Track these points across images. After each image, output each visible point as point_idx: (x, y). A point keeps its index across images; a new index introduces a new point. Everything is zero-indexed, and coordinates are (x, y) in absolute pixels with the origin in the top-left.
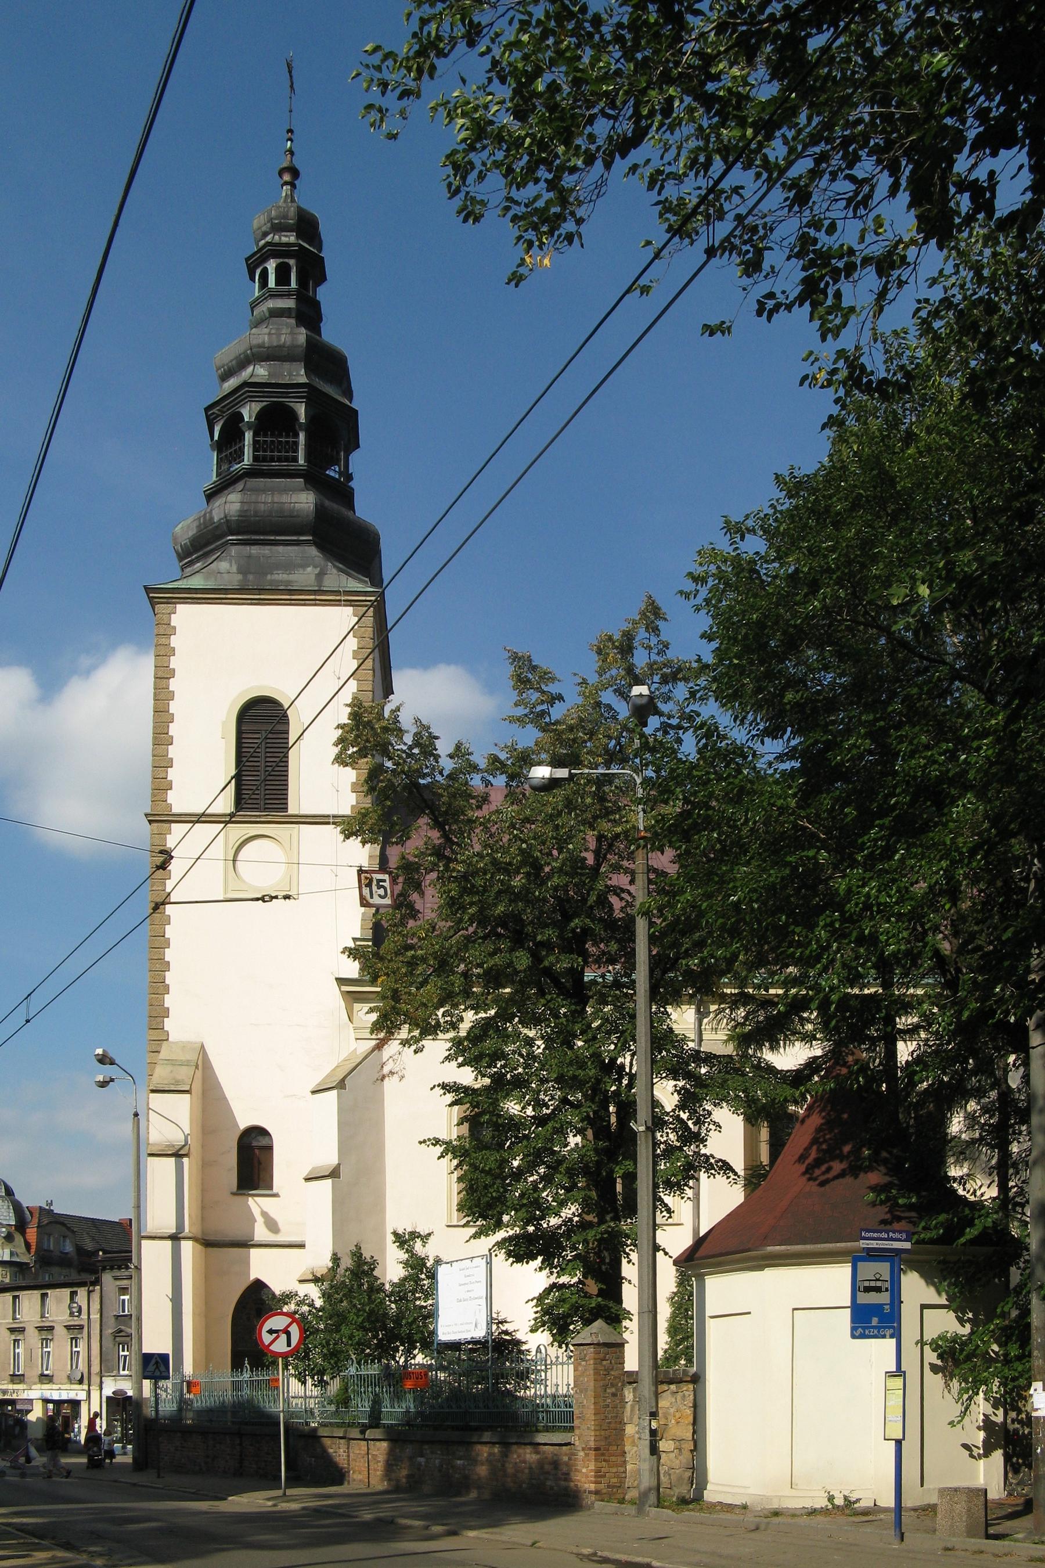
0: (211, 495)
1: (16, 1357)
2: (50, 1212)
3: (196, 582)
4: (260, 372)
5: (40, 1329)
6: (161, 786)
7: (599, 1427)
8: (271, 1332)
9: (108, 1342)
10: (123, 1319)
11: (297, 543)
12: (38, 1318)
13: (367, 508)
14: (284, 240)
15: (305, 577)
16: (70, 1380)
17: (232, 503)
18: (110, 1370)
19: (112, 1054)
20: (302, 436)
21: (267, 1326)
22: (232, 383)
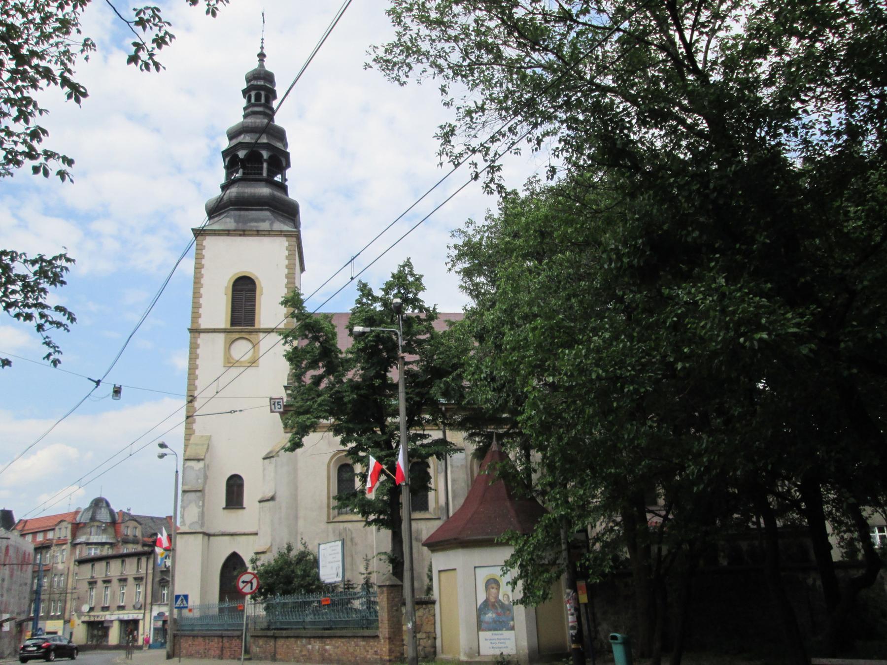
1: (106, 595)
2: (129, 514)
3: (216, 227)
4: (246, 138)
5: (135, 579)
6: (196, 316)
7: (390, 627)
8: (243, 582)
9: (156, 586)
10: (166, 572)
11: (262, 210)
14: (259, 83)
15: (265, 226)
16: (134, 607)
17: (233, 191)
18: (156, 601)
20: (265, 165)
21: (241, 580)
22: (235, 142)
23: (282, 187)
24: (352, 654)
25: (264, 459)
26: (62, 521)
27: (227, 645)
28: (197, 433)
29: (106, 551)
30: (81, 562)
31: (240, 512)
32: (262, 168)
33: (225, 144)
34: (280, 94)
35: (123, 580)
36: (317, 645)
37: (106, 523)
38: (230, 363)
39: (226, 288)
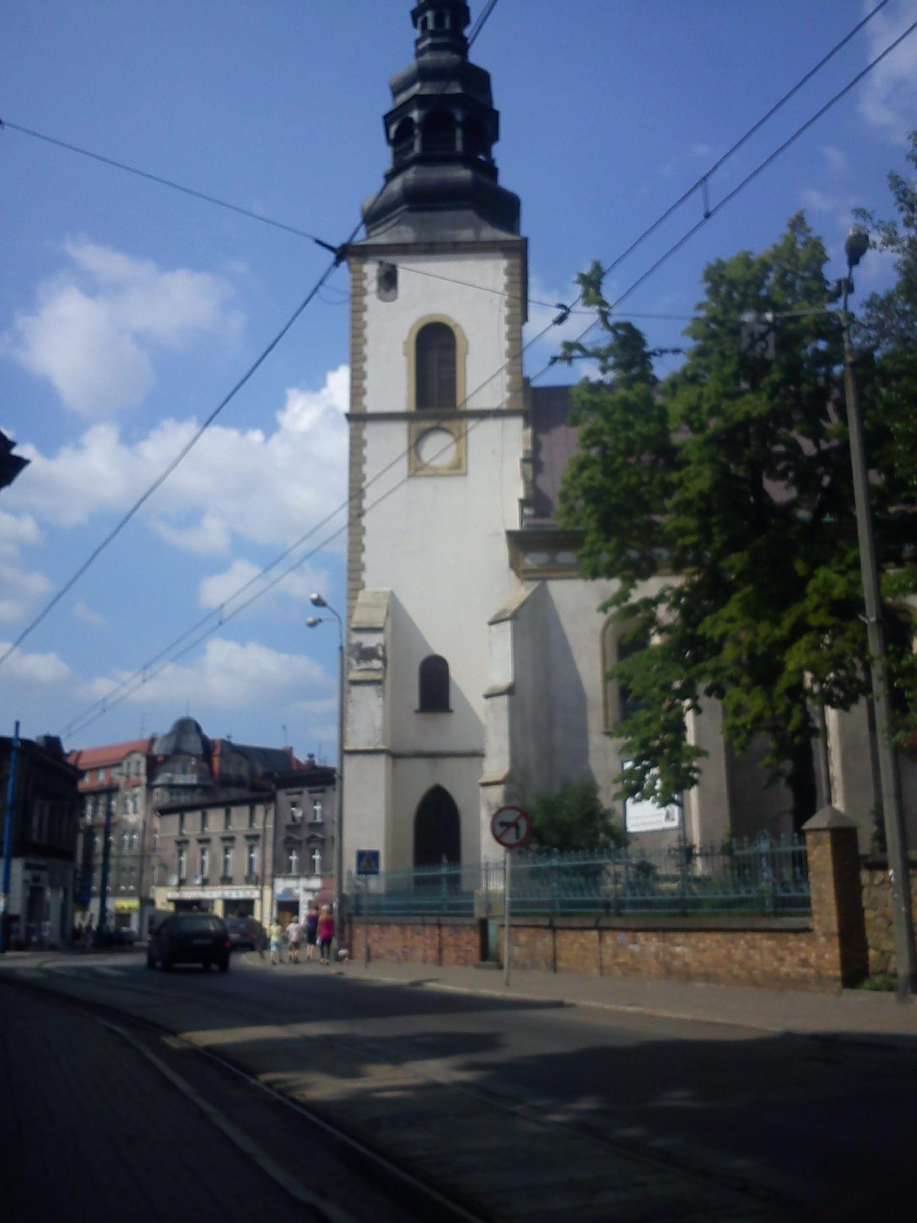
0: (389, 177)
3: (382, 238)
5: (248, 837)
12: (198, 831)
13: (506, 181)
15: (467, 235)
18: (280, 872)
19: (325, 598)
20: (459, 133)
22: (403, 98)
23: (491, 171)
24: (742, 964)
25: (492, 623)
26: (133, 752)
27: (450, 940)
28: (369, 588)
29: (197, 798)
30: (164, 811)
31: (442, 718)
32: (453, 140)
33: (387, 104)
34: (475, 15)
35: (228, 840)
36: (652, 944)
37: (196, 756)
38: (417, 468)
39: (406, 344)
